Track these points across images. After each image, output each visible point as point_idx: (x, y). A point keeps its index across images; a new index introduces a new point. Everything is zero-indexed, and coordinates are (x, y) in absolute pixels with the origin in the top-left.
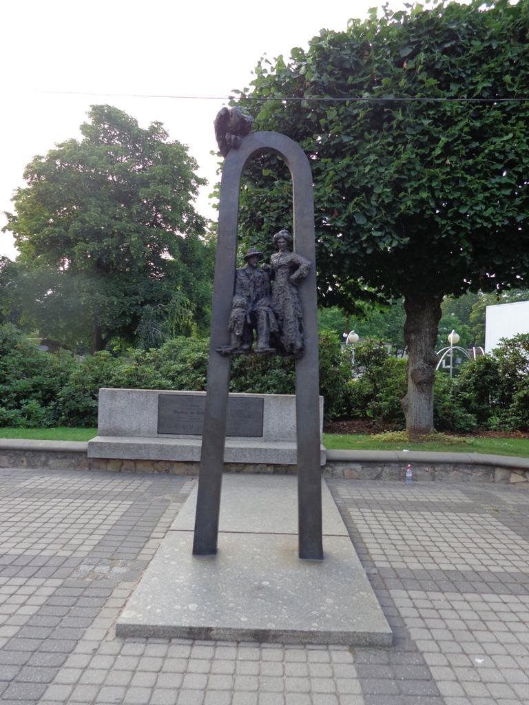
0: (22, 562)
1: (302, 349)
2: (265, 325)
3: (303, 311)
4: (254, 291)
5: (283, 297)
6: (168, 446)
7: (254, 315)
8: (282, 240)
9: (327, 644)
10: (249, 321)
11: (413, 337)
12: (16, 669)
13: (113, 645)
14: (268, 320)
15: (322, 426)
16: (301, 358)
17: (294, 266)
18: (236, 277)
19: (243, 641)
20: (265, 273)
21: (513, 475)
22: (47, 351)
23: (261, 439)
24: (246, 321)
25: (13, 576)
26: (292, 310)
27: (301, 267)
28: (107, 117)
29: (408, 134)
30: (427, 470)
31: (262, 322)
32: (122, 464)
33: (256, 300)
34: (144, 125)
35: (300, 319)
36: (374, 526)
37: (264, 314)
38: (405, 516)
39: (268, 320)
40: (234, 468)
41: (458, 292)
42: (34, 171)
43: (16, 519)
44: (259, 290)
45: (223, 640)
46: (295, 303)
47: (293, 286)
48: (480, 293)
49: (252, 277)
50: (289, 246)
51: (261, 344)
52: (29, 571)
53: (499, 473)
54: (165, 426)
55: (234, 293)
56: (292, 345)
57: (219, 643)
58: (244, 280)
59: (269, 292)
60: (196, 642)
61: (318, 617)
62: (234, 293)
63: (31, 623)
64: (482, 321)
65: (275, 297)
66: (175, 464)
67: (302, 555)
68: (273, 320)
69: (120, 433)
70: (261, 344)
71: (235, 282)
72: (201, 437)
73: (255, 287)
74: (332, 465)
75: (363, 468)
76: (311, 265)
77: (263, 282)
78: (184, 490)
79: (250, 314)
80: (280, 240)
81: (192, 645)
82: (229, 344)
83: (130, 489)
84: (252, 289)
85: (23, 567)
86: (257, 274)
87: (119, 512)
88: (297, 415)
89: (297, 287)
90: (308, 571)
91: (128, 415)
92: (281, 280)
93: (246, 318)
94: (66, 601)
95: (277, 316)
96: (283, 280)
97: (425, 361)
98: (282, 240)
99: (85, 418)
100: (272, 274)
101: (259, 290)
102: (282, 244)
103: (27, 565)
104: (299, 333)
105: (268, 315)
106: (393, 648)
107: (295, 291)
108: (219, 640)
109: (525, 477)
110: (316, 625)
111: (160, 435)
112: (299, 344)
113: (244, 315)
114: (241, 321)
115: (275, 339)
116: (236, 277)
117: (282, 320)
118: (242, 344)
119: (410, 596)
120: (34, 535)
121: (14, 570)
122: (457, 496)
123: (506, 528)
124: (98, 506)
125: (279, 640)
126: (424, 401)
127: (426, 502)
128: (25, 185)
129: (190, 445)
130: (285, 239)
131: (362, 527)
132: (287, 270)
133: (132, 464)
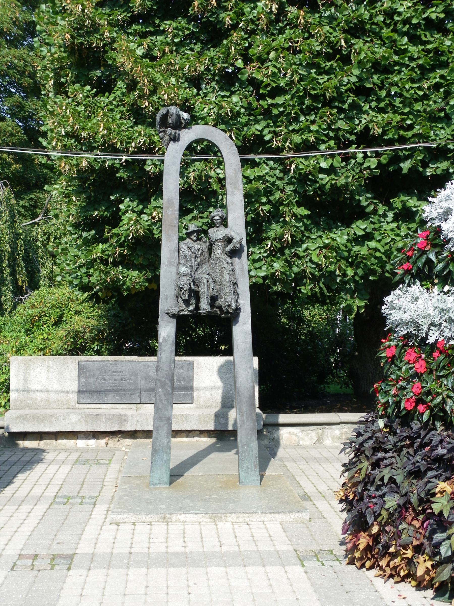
2: (206, 290)
5: (220, 266)
24: (190, 287)
26: (228, 276)
27: (235, 241)
29: (425, 247)
37: (205, 281)
41: (383, 303)
46: (230, 271)
48: (386, 299)
55: (179, 263)
77: (202, 253)
80: (216, 218)
84: (193, 260)
87: (32, 521)
92: (218, 251)
93: (190, 285)
102: (217, 221)
106: (28, 382)
113: (188, 282)
130: (219, 216)
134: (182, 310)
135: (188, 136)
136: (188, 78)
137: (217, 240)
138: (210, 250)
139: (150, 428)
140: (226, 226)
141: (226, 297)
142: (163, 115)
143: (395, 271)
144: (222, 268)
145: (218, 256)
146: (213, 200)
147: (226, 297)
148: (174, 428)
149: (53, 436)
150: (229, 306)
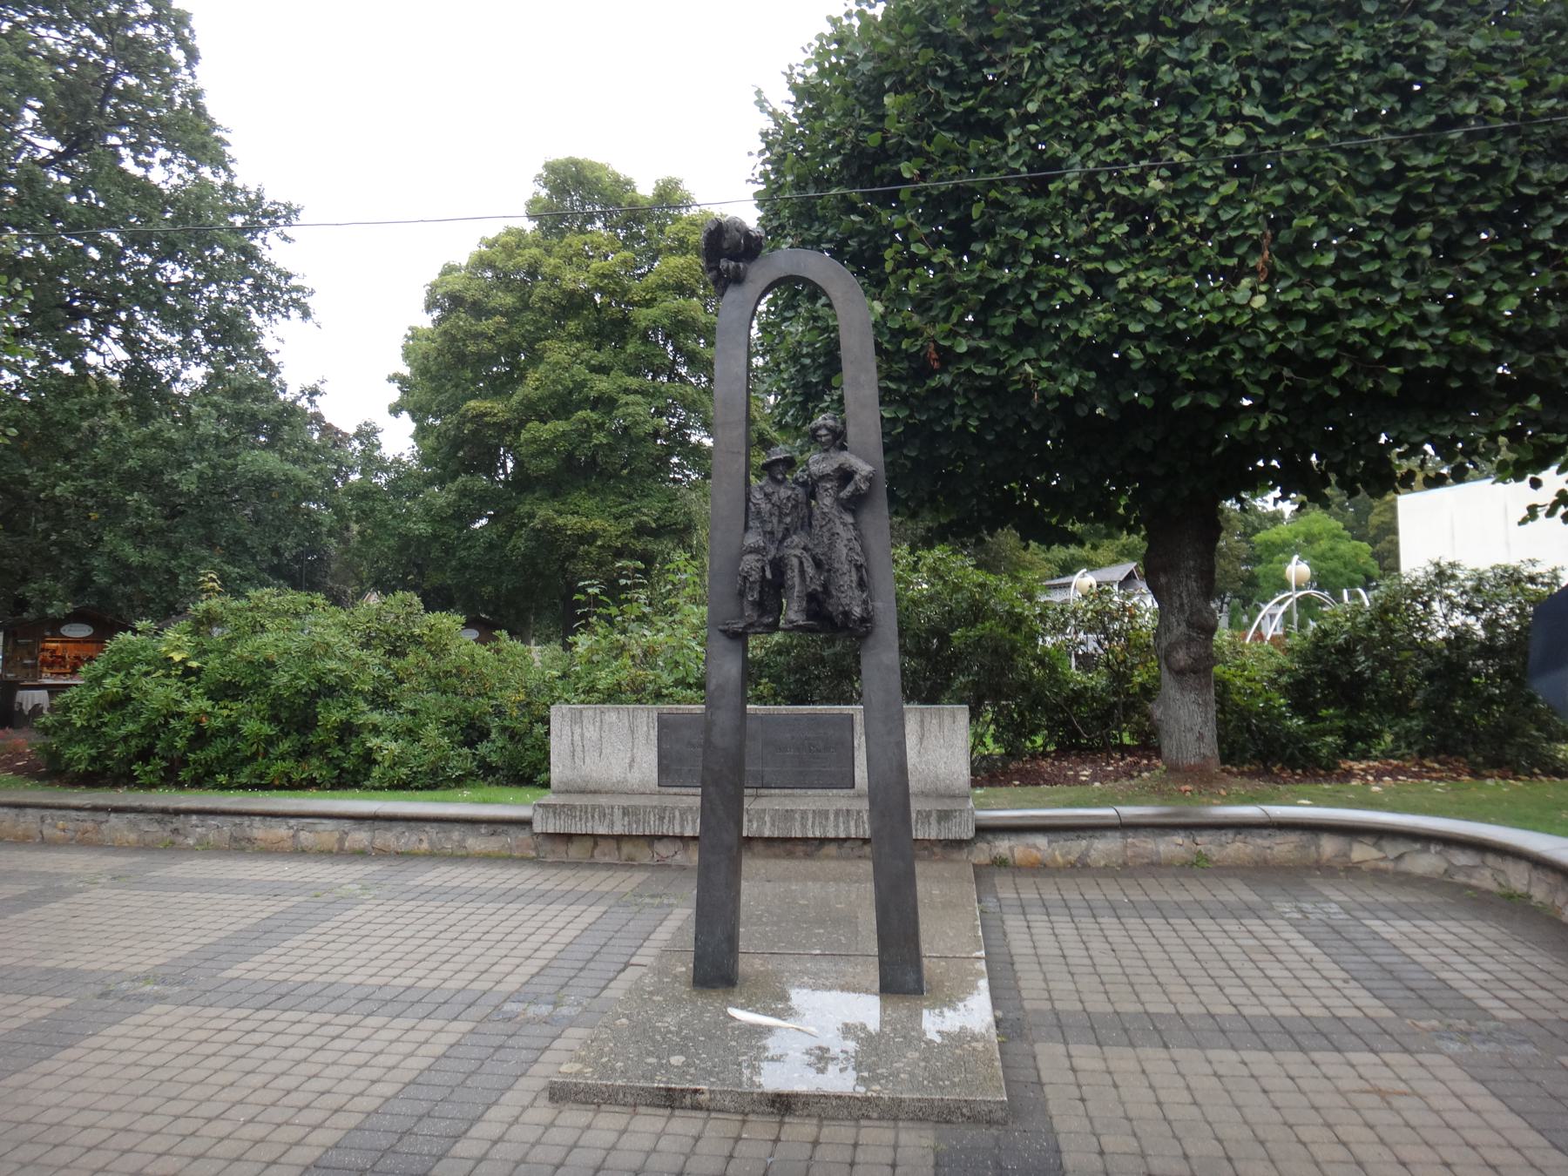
0: (412, 996)
1: (867, 619)
2: (797, 580)
3: (865, 550)
4: (780, 522)
7: (779, 566)
8: (823, 432)
9: (896, 1119)
10: (769, 575)
11: (1163, 580)
13: (543, 1112)
14: (802, 572)
15: (860, 741)
16: (868, 633)
18: (748, 500)
19: (753, 1111)
20: (799, 490)
22: (476, 641)
23: (851, 792)
24: (764, 576)
25: (398, 1016)
26: (845, 551)
27: (857, 477)
28: (574, 191)
30: (1180, 841)
31: (793, 577)
32: (596, 844)
33: (784, 538)
34: (645, 189)
35: (859, 568)
36: (1077, 961)
37: (795, 562)
39: (802, 572)
40: (800, 849)
42: (449, 300)
43: (407, 933)
44: (788, 520)
45: (720, 1111)
49: (775, 498)
50: (838, 439)
51: (793, 612)
52: (420, 1010)
55: (747, 528)
56: (847, 614)
57: (713, 1115)
58: (765, 507)
59: (807, 523)
60: (677, 1112)
61: (884, 1077)
62: (747, 528)
63: (420, 1080)
64: (1390, 529)
65: (816, 530)
70: (793, 612)
71: (747, 508)
73: (781, 516)
74: (990, 837)
75: (1050, 842)
76: (874, 473)
77: (795, 507)
79: (771, 562)
81: (669, 1118)
82: (741, 616)
83: (585, 887)
84: (775, 520)
85: (413, 1003)
86: (784, 492)
89: (854, 513)
91: (606, 751)
92: (826, 501)
94: (476, 1053)
95: (818, 564)
96: (828, 501)
97: (1190, 625)
98: (823, 432)
99: (526, 768)
100: (811, 488)
101: (788, 520)
103: (419, 1001)
104: (857, 593)
105: (801, 563)
107: (849, 519)
108: (715, 1110)
109: (1380, 850)
110: (878, 1088)
111: (663, 790)
112: (857, 611)
113: (759, 565)
114: (755, 576)
115: (817, 604)
116: (748, 500)
117: (829, 571)
118: (760, 616)
120: (434, 957)
121: (398, 1007)
123: (1483, 1003)
124: (542, 917)
125: (814, 1110)
126: (1194, 707)
128: (426, 321)
131: (1019, 944)
132: (835, 483)
133: (613, 844)
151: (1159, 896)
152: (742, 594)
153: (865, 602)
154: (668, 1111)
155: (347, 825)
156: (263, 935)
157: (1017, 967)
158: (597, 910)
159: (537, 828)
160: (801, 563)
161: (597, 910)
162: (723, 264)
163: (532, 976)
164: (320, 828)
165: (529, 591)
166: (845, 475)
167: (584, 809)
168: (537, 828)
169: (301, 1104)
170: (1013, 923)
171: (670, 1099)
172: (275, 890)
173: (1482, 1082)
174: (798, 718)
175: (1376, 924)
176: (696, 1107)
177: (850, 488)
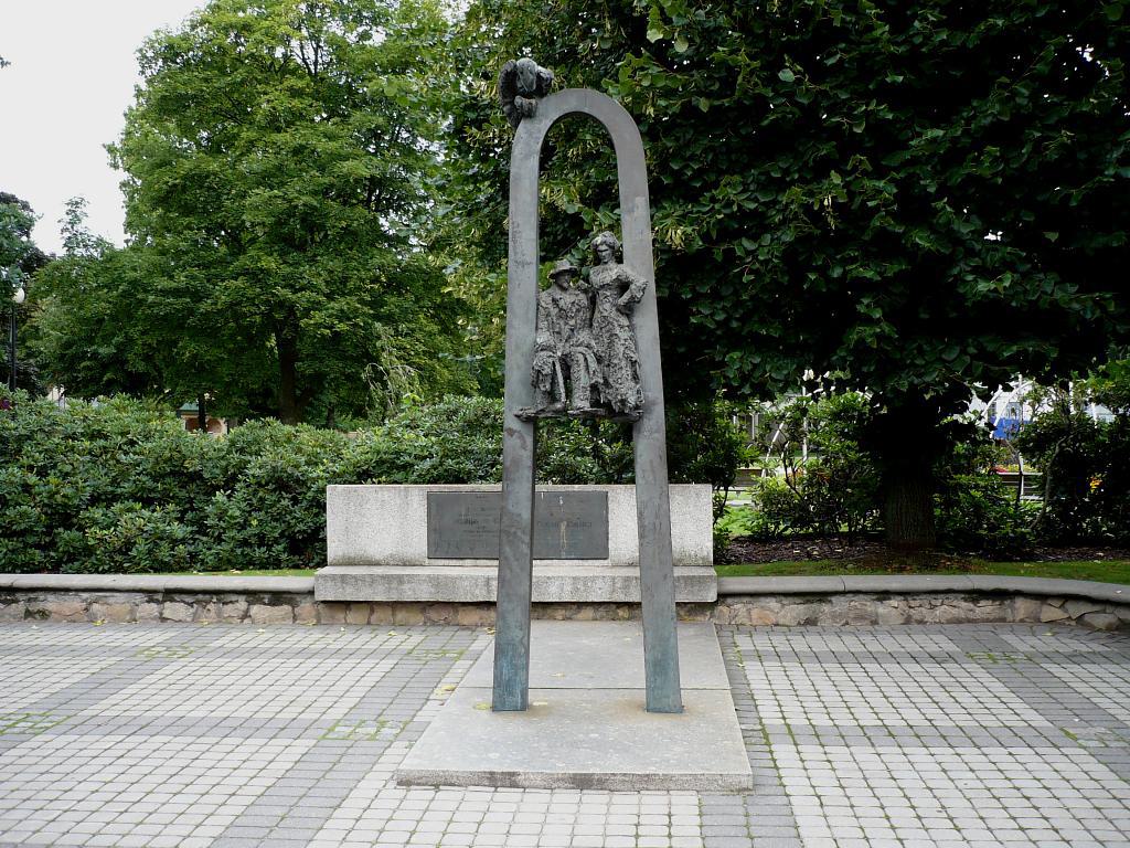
2: (583, 372)
6: (446, 577)
12: (134, 831)
14: (587, 367)
17: (623, 286)
20: (582, 296)
21: (1045, 608)
27: (633, 287)
37: (581, 357)
38: (929, 684)
47: (622, 314)
53: (1022, 607)
54: (444, 544)
66: (461, 609)
67: (495, 709)
68: (593, 365)
69: (160, 597)
72: (496, 563)
78: (477, 646)
79: (560, 359)
83: (373, 645)
88: (608, 533)
89: (629, 316)
90: (513, 725)
91: (377, 526)
92: (606, 307)
99: (307, 547)
107: (624, 321)
109: (1066, 611)
111: (433, 561)
112: (632, 400)
113: (551, 360)
119: (1057, 832)
122: (942, 643)
127: (1105, 663)
129: (474, 577)
134: (543, 410)
135: (551, 110)
136: (685, 431)
137: (602, 287)
138: (593, 302)
139: (494, 599)
140: (620, 260)
141: (618, 386)
142: (507, 74)
143: (1090, 372)
144: (611, 335)
145: (606, 314)
146: (884, 411)
147: (618, 386)
148: (533, 600)
149: (344, 607)
150: (623, 402)
151: (874, 647)
152: (535, 385)
153: (638, 392)
154: (493, 789)
155: (139, 597)
156: (98, 685)
157: (752, 686)
158: (387, 664)
159: (319, 597)
160: (586, 359)
161: (387, 664)
162: (518, 100)
163: (351, 709)
164: (111, 600)
165: (304, 374)
166: (623, 286)
167: (362, 579)
168: (319, 597)
169: (203, 792)
170: (753, 671)
171: (496, 780)
172: (105, 650)
173: (1105, 764)
174: (567, 494)
175: (1054, 668)
176: (514, 785)
177: (626, 297)
